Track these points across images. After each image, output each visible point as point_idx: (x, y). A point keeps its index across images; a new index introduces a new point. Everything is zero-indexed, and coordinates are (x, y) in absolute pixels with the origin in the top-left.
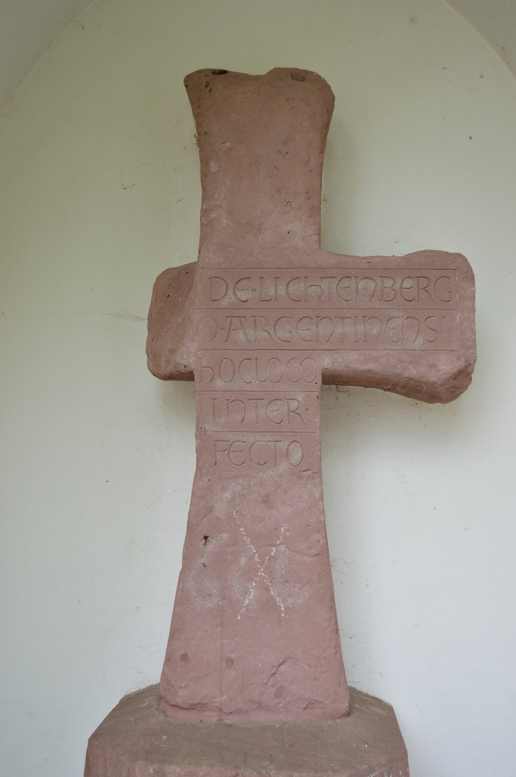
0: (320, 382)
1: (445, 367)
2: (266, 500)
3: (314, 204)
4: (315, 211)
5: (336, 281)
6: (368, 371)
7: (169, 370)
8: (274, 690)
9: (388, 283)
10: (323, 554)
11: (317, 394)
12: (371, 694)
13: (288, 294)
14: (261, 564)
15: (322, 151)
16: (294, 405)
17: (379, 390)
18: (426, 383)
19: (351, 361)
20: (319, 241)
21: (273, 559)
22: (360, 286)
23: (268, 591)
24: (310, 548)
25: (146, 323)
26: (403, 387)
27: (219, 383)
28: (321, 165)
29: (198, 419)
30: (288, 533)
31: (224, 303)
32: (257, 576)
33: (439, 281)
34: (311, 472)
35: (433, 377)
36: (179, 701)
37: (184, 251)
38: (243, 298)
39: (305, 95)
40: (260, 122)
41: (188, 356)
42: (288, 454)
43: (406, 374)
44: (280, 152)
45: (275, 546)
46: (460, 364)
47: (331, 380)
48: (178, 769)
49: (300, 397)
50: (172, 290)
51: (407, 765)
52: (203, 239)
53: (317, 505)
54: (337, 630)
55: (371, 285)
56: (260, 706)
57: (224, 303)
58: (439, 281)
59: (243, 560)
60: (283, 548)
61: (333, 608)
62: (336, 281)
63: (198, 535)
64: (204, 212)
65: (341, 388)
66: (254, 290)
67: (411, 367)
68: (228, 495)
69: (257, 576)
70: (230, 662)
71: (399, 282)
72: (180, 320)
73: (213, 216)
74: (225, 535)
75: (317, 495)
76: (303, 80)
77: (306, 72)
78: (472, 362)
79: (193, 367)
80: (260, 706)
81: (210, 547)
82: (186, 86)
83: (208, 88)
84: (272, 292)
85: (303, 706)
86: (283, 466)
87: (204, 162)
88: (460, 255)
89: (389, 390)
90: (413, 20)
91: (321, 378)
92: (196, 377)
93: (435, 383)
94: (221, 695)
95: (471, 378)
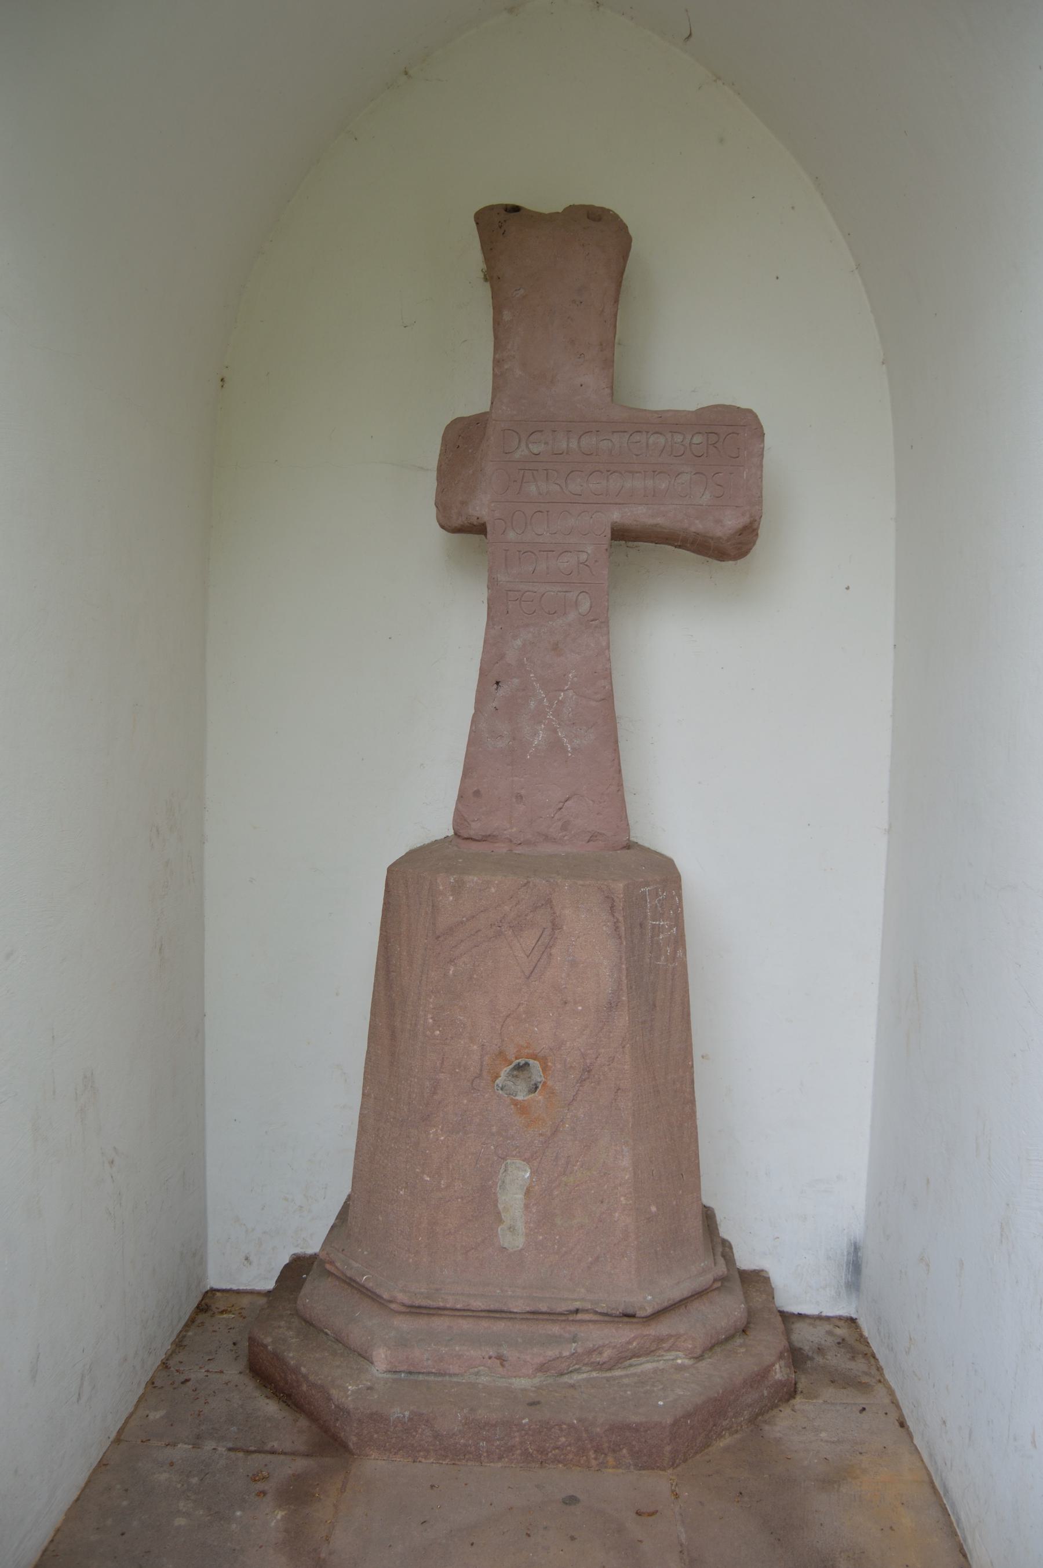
0: (609, 535)
1: (731, 522)
2: (555, 648)
3: (607, 353)
4: (609, 363)
5: (627, 436)
6: (656, 525)
7: (457, 522)
8: (560, 824)
9: (678, 438)
10: (608, 699)
11: (606, 547)
12: (653, 848)
13: (580, 447)
14: (550, 707)
15: (616, 301)
16: (583, 557)
17: (667, 547)
18: (712, 538)
19: (639, 515)
20: (612, 394)
21: (561, 702)
22: (651, 441)
23: (557, 733)
24: (596, 693)
25: (435, 474)
26: (692, 543)
27: (511, 535)
28: (616, 315)
29: (490, 570)
30: (575, 679)
31: (517, 456)
32: (546, 718)
33: (729, 436)
34: (598, 621)
35: (719, 532)
36: (472, 833)
37: (474, 397)
38: (536, 451)
39: (599, 232)
40: (551, 263)
41: (481, 508)
42: (576, 604)
43: (693, 529)
44: (574, 301)
45: (563, 691)
46: (745, 520)
47: (621, 535)
48: (475, 879)
49: (590, 549)
50: (463, 441)
51: (680, 888)
52: (496, 389)
53: (604, 653)
54: (620, 771)
55: (662, 440)
56: (547, 838)
57: (517, 456)
58: (729, 436)
59: (532, 704)
60: (570, 693)
61: (616, 750)
62: (627, 436)
63: (491, 678)
64: (497, 363)
65: (630, 544)
66: (546, 443)
67: (697, 522)
68: (519, 642)
69: (546, 718)
70: (519, 797)
71: (689, 437)
72: (471, 472)
73: (506, 367)
74: (516, 681)
75: (604, 644)
76: (600, 220)
77: (603, 209)
78: (757, 518)
79: (486, 519)
80: (547, 838)
81: (501, 692)
82: (477, 224)
83: (501, 225)
84: (565, 446)
85: (587, 838)
86: (572, 616)
87: (497, 310)
88: (750, 411)
89: (680, 547)
90: (722, 141)
91: (609, 532)
92: (488, 529)
93: (720, 538)
94: (511, 828)
95: (757, 535)
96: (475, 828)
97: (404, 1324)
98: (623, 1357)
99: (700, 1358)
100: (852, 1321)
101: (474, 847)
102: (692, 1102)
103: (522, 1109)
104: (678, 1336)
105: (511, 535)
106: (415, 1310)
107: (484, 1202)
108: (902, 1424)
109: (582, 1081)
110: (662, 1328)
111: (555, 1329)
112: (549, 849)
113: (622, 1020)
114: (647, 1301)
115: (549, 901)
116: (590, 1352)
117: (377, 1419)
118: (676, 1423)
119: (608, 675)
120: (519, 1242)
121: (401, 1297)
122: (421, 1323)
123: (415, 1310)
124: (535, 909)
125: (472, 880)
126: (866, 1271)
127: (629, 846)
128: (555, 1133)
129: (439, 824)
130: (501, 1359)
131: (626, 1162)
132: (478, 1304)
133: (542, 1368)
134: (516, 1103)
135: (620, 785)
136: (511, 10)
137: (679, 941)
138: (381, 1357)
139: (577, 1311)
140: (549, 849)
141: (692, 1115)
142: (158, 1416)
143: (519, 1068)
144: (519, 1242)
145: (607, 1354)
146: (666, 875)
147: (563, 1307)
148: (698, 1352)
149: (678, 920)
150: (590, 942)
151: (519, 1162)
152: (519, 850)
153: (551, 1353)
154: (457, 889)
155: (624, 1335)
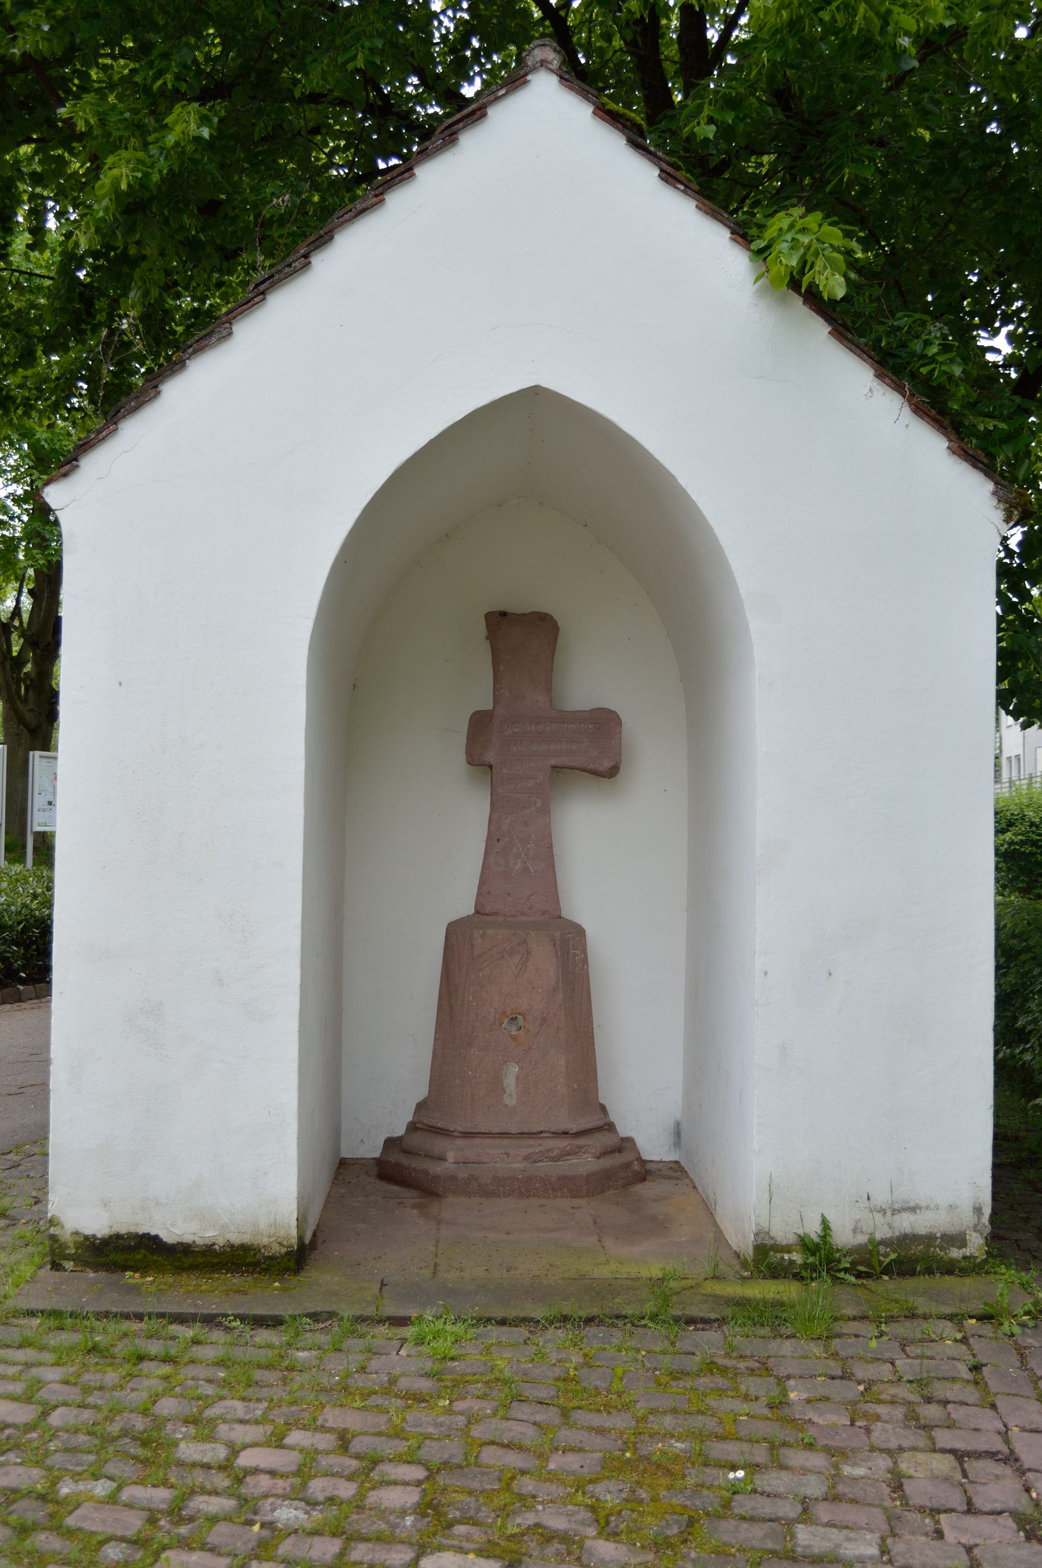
1: (607, 764)
2: (526, 824)
4: (549, 690)
10: (550, 847)
15: (553, 660)
19: (564, 760)
27: (504, 771)
33: (604, 724)
34: (545, 811)
35: (601, 769)
37: (486, 703)
39: (541, 628)
46: (614, 763)
50: (480, 725)
53: (548, 826)
55: (574, 727)
56: (522, 914)
58: (604, 724)
61: (554, 872)
63: (492, 839)
70: (509, 894)
80: (522, 914)
81: (500, 845)
83: (498, 622)
86: (533, 808)
96: (488, 909)
97: (460, 1142)
98: (564, 1155)
99: (598, 1158)
100: (677, 1162)
101: (488, 918)
102: (593, 1038)
103: (514, 1038)
104: (588, 1146)
105: (504, 771)
106: (466, 1135)
107: (497, 1084)
108: (694, 1187)
109: (541, 1025)
110: (581, 1141)
111: (532, 1142)
112: (522, 919)
113: (560, 996)
114: (574, 1128)
115: (525, 942)
116: (548, 1151)
117: (453, 1178)
118: (588, 1175)
119: (550, 836)
120: (514, 1102)
121: (459, 1129)
122: (468, 1141)
123: (466, 1135)
124: (519, 945)
125: (490, 932)
126: (682, 1134)
127: (560, 917)
128: (530, 1049)
129: (467, 908)
130: (507, 1154)
131: (562, 1062)
132: (495, 1130)
133: (526, 1158)
134: (511, 1036)
135: (556, 888)
136: (499, 506)
137: (585, 961)
138: (451, 1156)
139: (541, 1132)
140: (522, 919)
141: (593, 1044)
142: (1016, 304)
143: (513, 1019)
144: (514, 1102)
145: (556, 1152)
146: (580, 932)
147: (534, 1130)
148: (598, 1154)
149: (584, 951)
150: (544, 963)
151: (513, 1064)
152: (509, 919)
153: (530, 1151)
154: (483, 936)
155: (564, 1143)
